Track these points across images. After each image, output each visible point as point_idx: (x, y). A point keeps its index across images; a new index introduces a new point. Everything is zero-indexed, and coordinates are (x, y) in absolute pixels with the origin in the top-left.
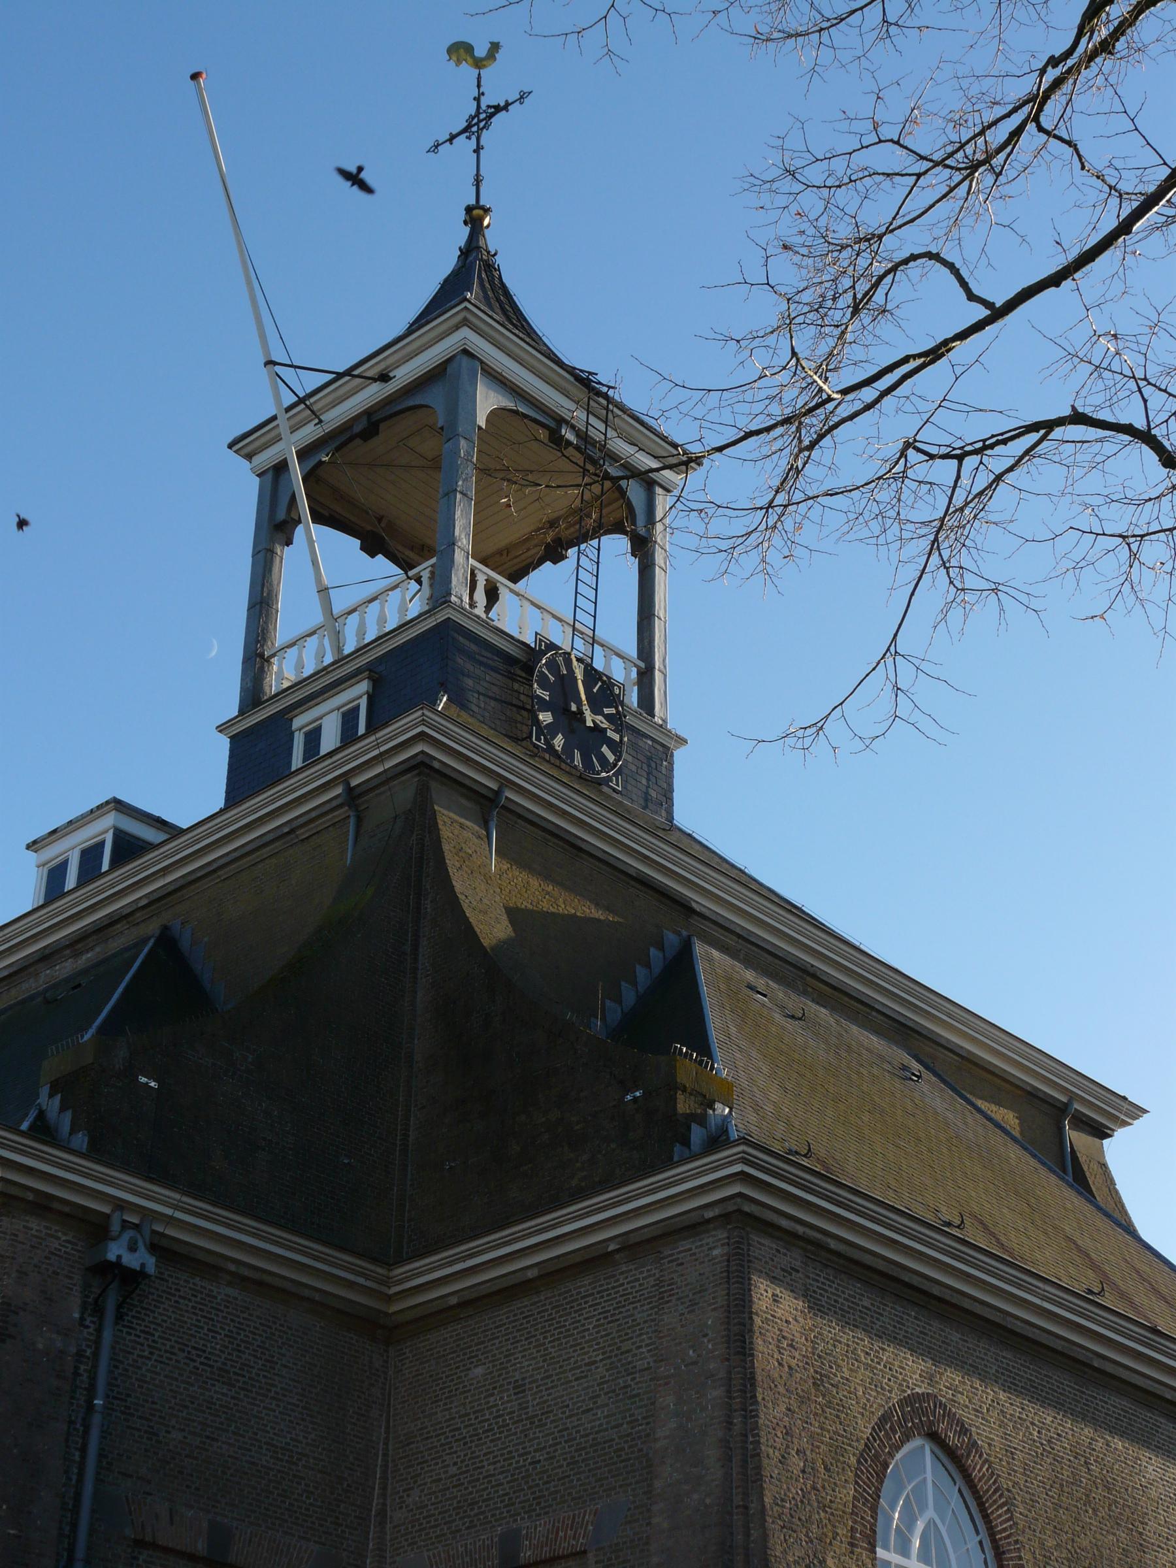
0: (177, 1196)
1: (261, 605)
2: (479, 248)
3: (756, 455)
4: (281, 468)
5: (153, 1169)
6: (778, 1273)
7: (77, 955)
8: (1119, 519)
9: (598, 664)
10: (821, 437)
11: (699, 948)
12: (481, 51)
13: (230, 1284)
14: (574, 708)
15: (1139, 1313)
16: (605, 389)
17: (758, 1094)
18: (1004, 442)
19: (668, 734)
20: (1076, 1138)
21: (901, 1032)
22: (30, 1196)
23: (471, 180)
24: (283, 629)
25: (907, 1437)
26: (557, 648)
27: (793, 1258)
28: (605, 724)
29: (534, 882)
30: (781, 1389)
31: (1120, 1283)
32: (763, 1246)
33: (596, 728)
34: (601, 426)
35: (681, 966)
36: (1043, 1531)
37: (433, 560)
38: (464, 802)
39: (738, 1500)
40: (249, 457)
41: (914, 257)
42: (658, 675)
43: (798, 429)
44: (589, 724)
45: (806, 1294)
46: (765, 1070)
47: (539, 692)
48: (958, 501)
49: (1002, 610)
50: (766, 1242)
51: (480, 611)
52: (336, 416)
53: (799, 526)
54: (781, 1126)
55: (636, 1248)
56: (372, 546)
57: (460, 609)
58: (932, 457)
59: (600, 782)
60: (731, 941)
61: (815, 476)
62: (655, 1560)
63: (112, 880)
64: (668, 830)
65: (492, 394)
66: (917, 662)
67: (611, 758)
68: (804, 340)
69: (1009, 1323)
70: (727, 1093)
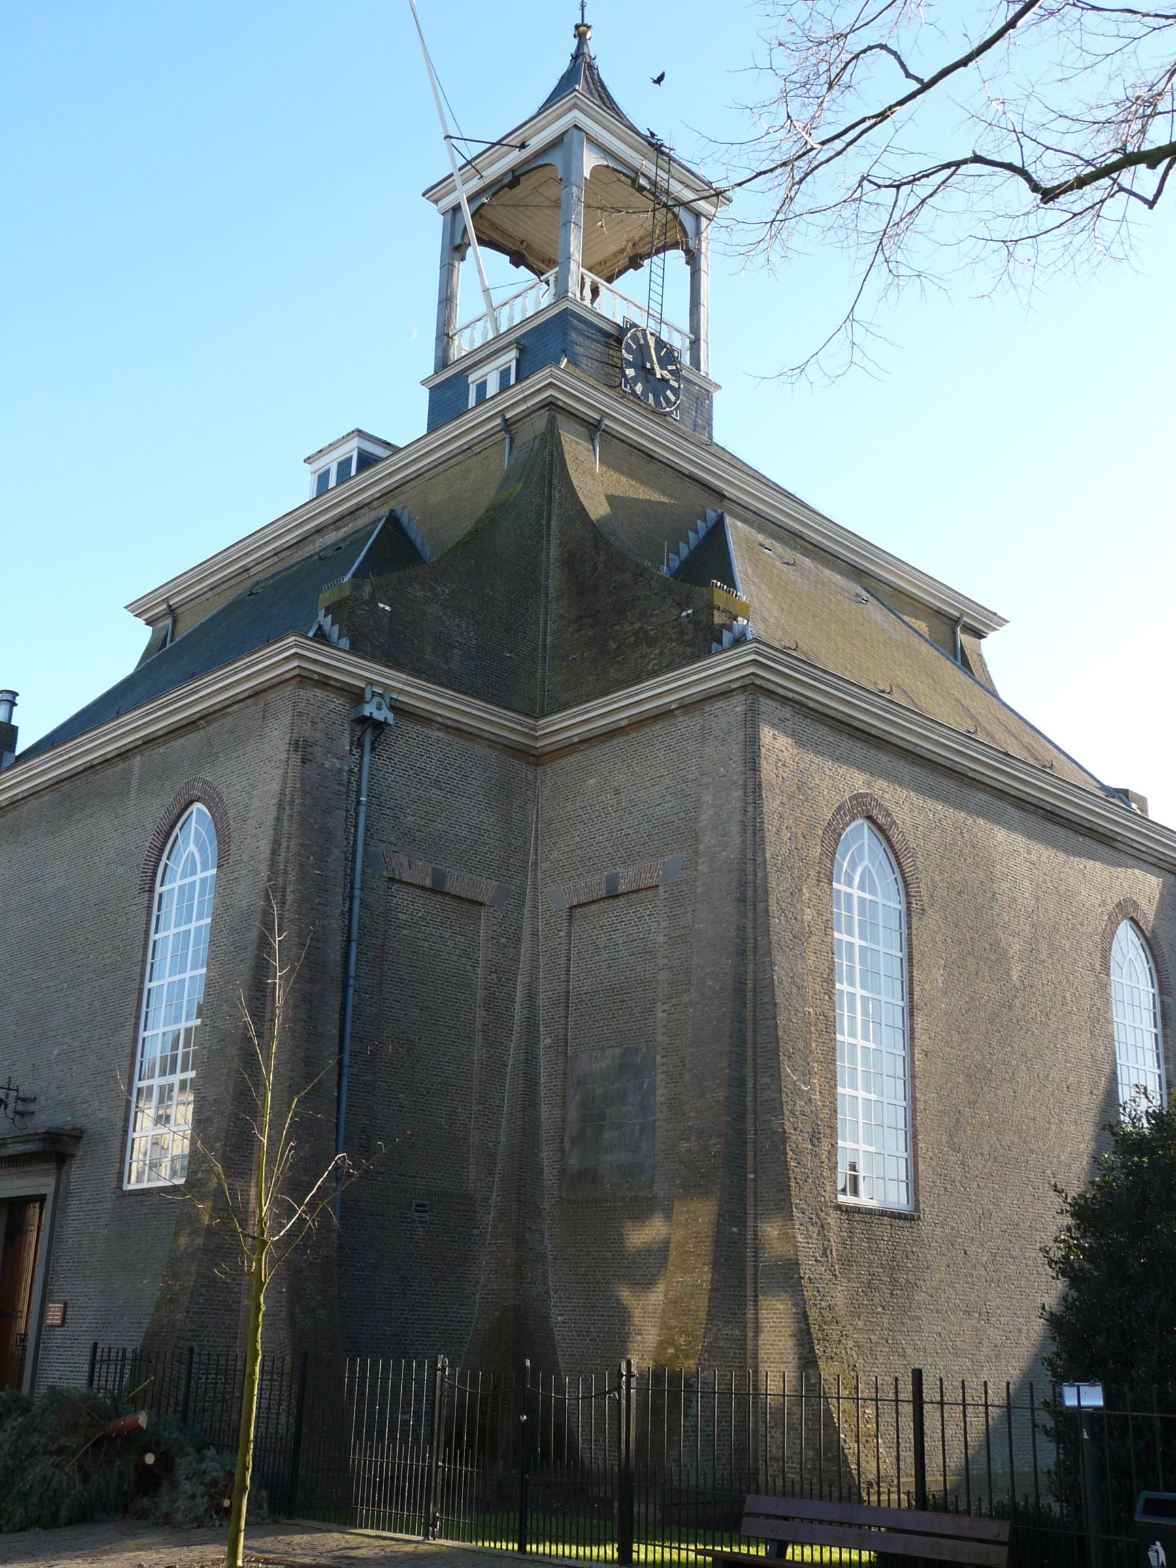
0: (405, 676)
1: (447, 301)
2: (583, 54)
3: (764, 188)
4: (457, 209)
5: (390, 660)
6: (776, 721)
7: (338, 529)
8: (1002, 228)
9: (664, 337)
10: (807, 175)
11: (728, 520)
13: (439, 730)
14: (648, 366)
15: (997, 744)
16: (667, 151)
17: (765, 611)
18: (927, 176)
19: (710, 382)
20: (963, 638)
21: (857, 573)
22: (316, 677)
23: (579, 6)
24: (461, 318)
25: (853, 819)
26: (637, 326)
27: (786, 712)
28: (668, 376)
29: (624, 479)
30: (777, 791)
31: (987, 727)
32: (767, 705)
33: (663, 379)
34: (666, 176)
35: (718, 530)
36: (933, 872)
37: (557, 269)
38: (579, 428)
39: (750, 856)
40: (436, 202)
41: (870, 48)
42: (702, 342)
43: (792, 169)
44: (659, 376)
45: (793, 735)
46: (770, 596)
47: (626, 355)
48: (896, 218)
49: (923, 290)
50: (769, 702)
51: (587, 302)
52: (492, 172)
53: (790, 235)
54: (780, 632)
55: (688, 707)
56: (518, 260)
57: (575, 302)
58: (879, 186)
59: (665, 415)
60: (749, 515)
61: (802, 202)
62: (699, 890)
63: (359, 481)
64: (708, 445)
65: (594, 155)
66: (866, 325)
67: (673, 398)
68: (794, 107)
69: (918, 751)
70: (745, 611)
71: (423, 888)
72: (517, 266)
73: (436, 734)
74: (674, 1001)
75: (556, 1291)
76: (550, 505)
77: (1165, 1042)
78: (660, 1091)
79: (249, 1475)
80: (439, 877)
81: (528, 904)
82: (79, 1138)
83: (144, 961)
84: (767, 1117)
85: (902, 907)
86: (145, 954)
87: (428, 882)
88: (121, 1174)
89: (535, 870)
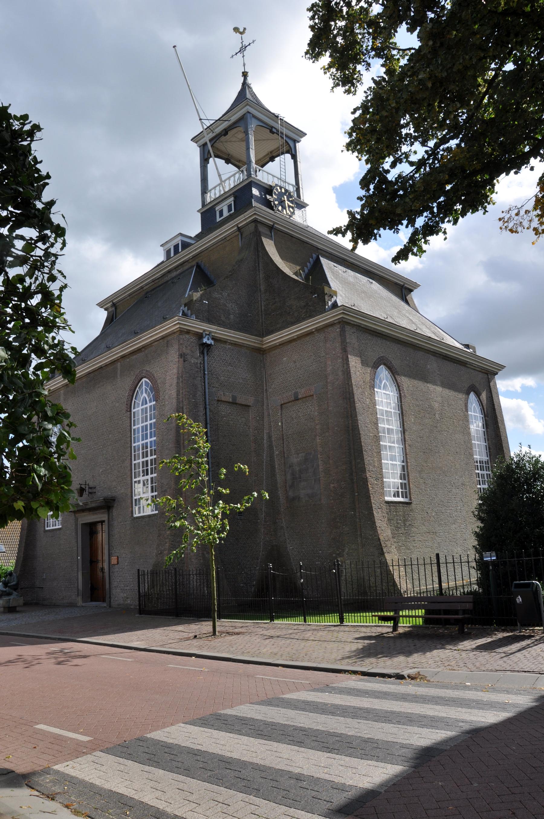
5: (209, 320)
6: (351, 333)
7: (176, 271)
12: (241, 30)
23: (243, 64)
24: (210, 186)
32: (348, 328)
40: (196, 142)
42: (301, 189)
60: (327, 255)
71: (229, 402)
72: (228, 164)
73: (228, 346)
74: (323, 435)
75: (288, 539)
76: (258, 258)
77: (487, 434)
78: (321, 467)
79: (216, 606)
80: (234, 398)
81: (265, 404)
82: (114, 500)
83: (131, 436)
84: (360, 473)
85: (398, 395)
86: (131, 434)
87: (231, 400)
88: (132, 511)
89: (267, 392)
